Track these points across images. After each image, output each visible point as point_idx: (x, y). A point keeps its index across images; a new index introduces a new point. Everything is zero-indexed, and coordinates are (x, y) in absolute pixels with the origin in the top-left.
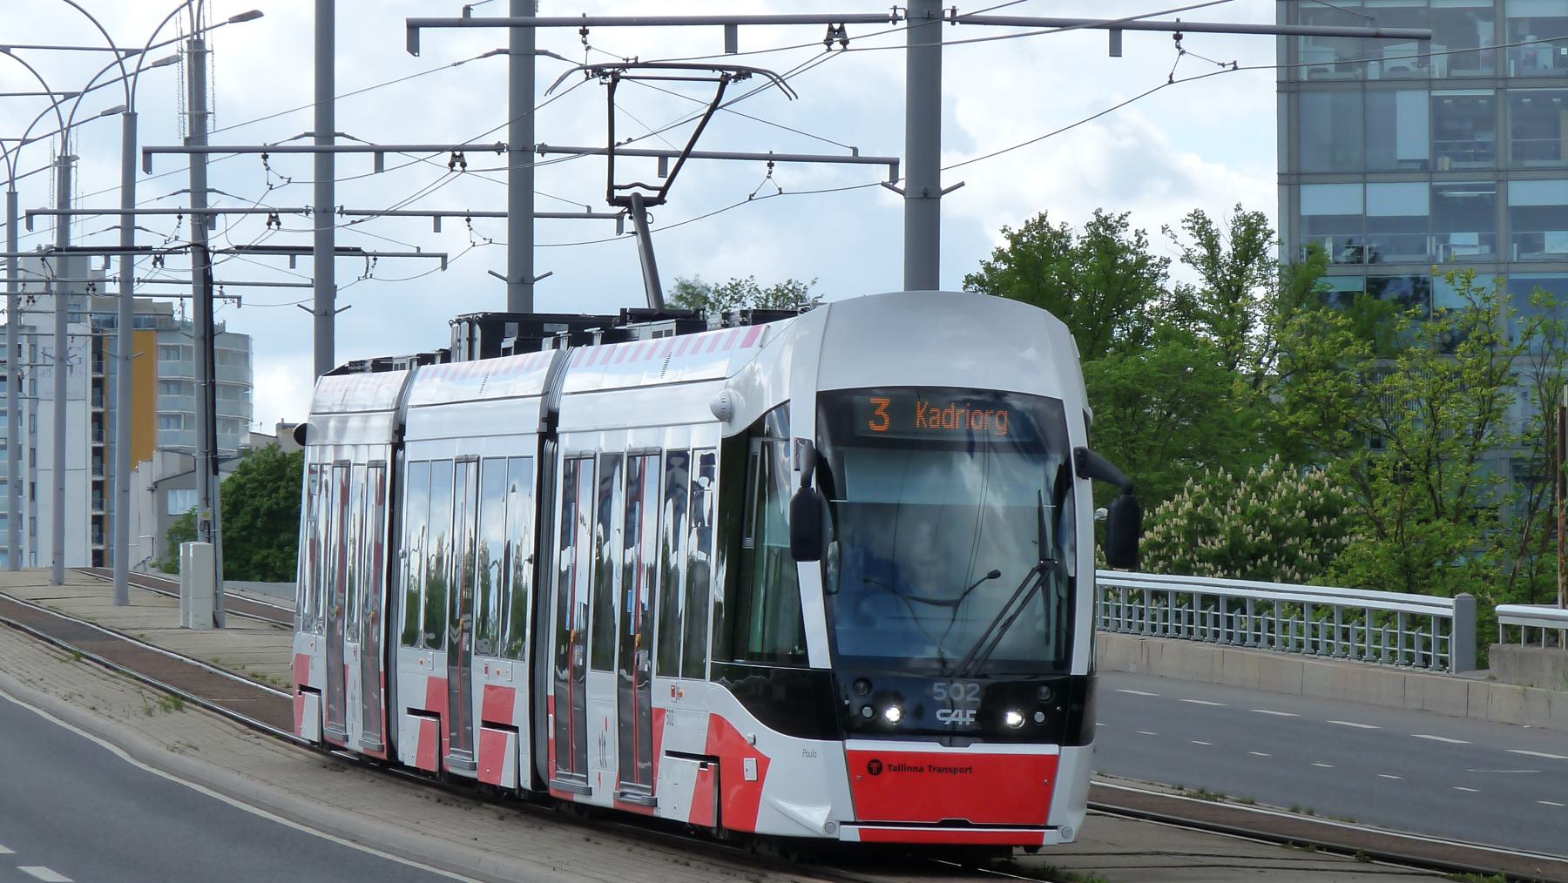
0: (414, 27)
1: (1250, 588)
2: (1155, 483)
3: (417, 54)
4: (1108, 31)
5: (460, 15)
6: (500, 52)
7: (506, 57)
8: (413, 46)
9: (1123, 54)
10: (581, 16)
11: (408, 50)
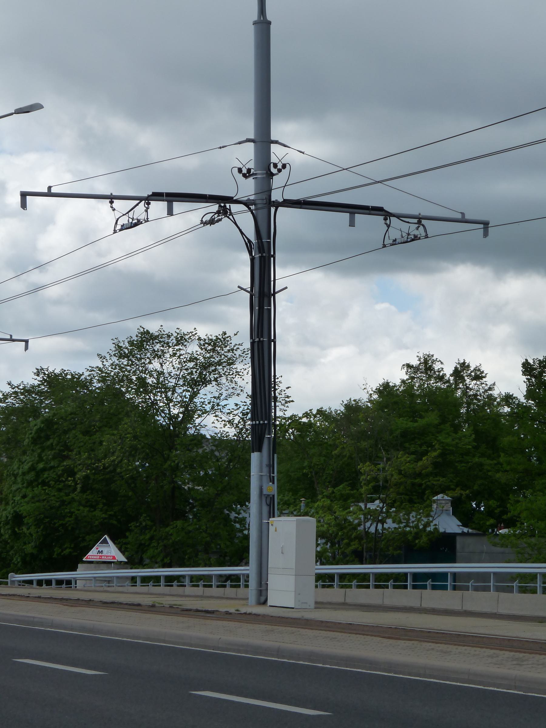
0: (24, 195)
1: (154, 572)
2: (422, 471)
3: (25, 209)
4: (349, 214)
5: (46, 191)
6: (248, 140)
7: (252, 145)
8: (24, 205)
9: (355, 226)
10: (110, 194)
11: (21, 207)
